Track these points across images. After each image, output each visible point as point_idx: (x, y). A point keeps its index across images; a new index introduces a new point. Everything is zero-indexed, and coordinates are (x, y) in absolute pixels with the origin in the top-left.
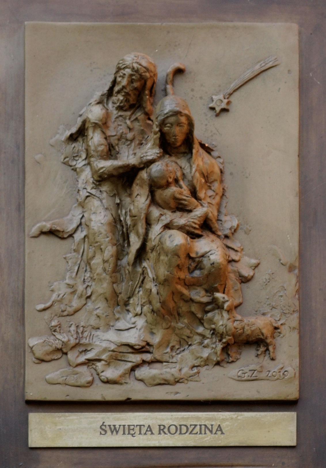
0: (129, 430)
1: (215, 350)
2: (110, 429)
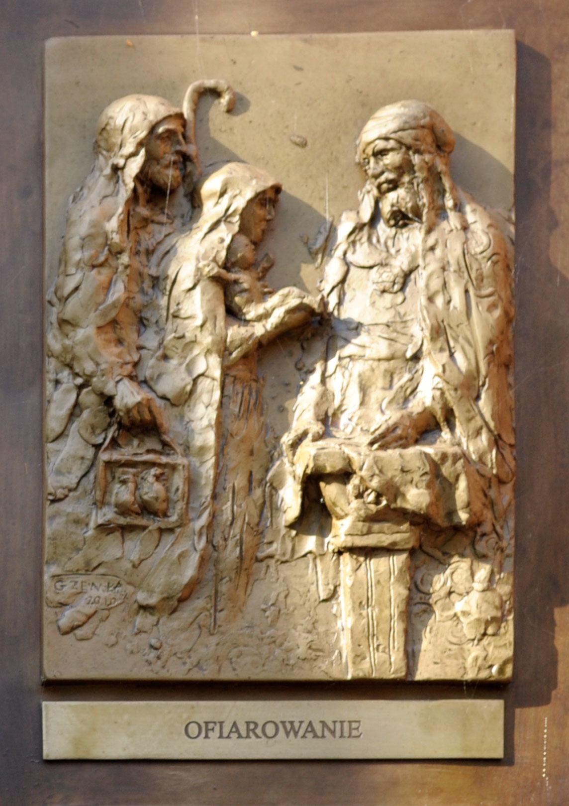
1: (87, 519)
2: (285, 727)
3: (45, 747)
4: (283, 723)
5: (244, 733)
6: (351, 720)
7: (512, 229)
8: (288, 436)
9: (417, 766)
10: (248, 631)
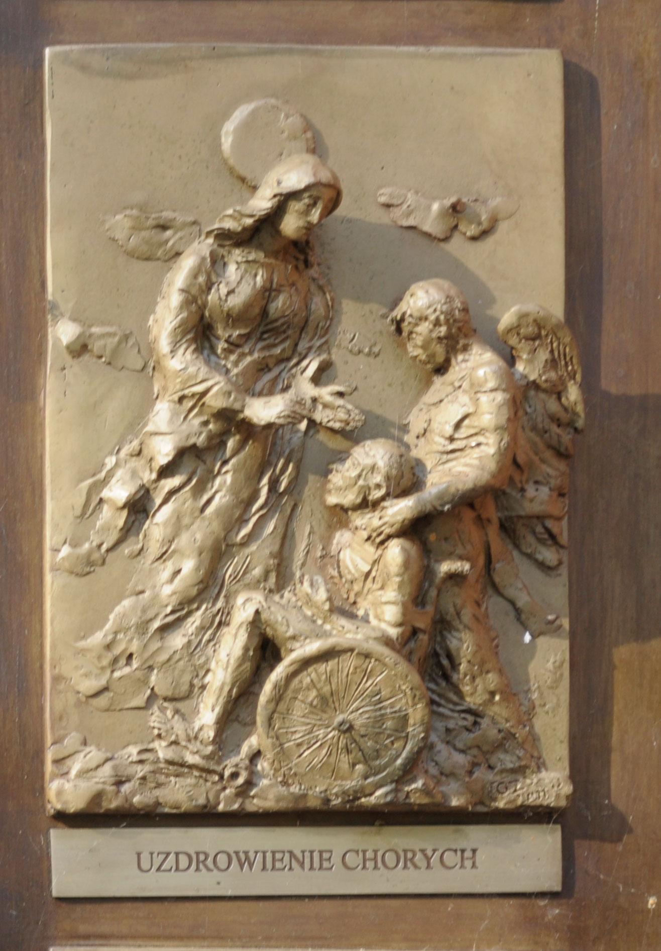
0: (199, 860)
2: (239, 860)
4: (237, 853)
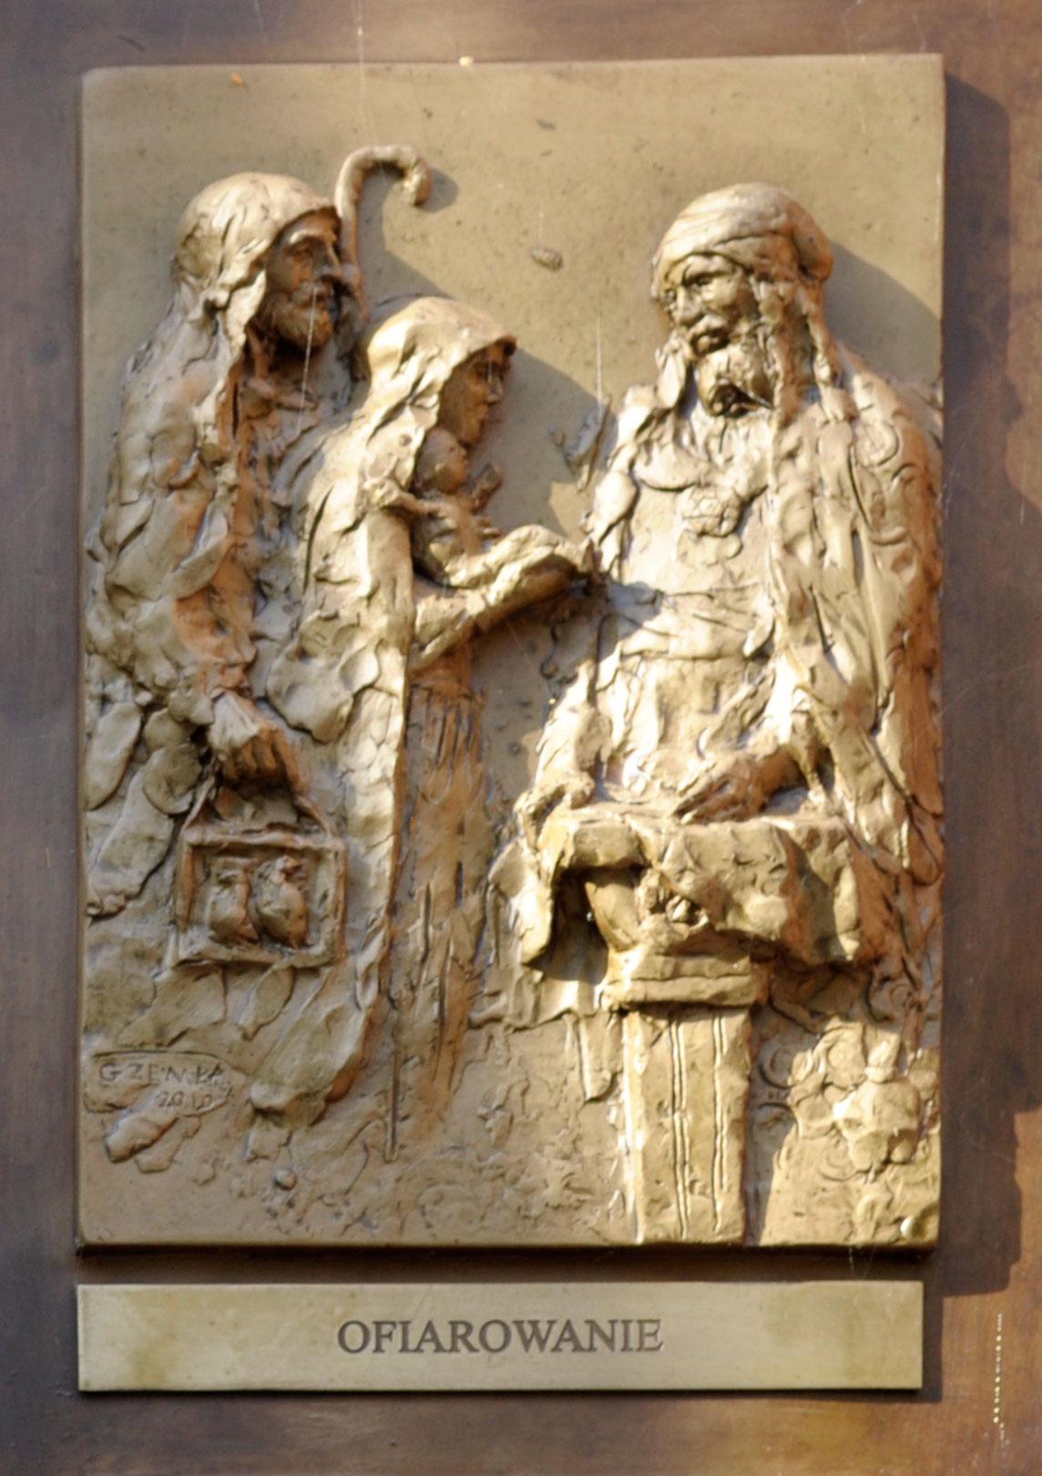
1: (160, 951)
2: (521, 1332)
3: (82, 1369)
4: (519, 1323)
5: (446, 1343)
6: (643, 1318)
7: (938, 419)
8: (527, 799)
9: (763, 1403)
10: (454, 1156)
